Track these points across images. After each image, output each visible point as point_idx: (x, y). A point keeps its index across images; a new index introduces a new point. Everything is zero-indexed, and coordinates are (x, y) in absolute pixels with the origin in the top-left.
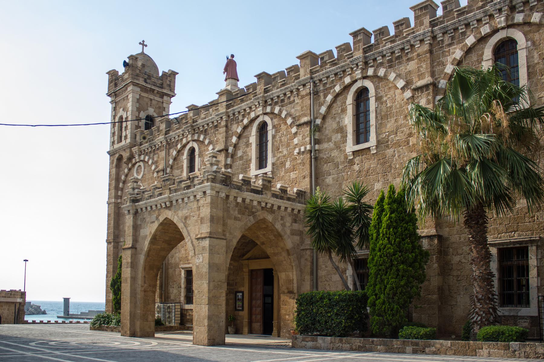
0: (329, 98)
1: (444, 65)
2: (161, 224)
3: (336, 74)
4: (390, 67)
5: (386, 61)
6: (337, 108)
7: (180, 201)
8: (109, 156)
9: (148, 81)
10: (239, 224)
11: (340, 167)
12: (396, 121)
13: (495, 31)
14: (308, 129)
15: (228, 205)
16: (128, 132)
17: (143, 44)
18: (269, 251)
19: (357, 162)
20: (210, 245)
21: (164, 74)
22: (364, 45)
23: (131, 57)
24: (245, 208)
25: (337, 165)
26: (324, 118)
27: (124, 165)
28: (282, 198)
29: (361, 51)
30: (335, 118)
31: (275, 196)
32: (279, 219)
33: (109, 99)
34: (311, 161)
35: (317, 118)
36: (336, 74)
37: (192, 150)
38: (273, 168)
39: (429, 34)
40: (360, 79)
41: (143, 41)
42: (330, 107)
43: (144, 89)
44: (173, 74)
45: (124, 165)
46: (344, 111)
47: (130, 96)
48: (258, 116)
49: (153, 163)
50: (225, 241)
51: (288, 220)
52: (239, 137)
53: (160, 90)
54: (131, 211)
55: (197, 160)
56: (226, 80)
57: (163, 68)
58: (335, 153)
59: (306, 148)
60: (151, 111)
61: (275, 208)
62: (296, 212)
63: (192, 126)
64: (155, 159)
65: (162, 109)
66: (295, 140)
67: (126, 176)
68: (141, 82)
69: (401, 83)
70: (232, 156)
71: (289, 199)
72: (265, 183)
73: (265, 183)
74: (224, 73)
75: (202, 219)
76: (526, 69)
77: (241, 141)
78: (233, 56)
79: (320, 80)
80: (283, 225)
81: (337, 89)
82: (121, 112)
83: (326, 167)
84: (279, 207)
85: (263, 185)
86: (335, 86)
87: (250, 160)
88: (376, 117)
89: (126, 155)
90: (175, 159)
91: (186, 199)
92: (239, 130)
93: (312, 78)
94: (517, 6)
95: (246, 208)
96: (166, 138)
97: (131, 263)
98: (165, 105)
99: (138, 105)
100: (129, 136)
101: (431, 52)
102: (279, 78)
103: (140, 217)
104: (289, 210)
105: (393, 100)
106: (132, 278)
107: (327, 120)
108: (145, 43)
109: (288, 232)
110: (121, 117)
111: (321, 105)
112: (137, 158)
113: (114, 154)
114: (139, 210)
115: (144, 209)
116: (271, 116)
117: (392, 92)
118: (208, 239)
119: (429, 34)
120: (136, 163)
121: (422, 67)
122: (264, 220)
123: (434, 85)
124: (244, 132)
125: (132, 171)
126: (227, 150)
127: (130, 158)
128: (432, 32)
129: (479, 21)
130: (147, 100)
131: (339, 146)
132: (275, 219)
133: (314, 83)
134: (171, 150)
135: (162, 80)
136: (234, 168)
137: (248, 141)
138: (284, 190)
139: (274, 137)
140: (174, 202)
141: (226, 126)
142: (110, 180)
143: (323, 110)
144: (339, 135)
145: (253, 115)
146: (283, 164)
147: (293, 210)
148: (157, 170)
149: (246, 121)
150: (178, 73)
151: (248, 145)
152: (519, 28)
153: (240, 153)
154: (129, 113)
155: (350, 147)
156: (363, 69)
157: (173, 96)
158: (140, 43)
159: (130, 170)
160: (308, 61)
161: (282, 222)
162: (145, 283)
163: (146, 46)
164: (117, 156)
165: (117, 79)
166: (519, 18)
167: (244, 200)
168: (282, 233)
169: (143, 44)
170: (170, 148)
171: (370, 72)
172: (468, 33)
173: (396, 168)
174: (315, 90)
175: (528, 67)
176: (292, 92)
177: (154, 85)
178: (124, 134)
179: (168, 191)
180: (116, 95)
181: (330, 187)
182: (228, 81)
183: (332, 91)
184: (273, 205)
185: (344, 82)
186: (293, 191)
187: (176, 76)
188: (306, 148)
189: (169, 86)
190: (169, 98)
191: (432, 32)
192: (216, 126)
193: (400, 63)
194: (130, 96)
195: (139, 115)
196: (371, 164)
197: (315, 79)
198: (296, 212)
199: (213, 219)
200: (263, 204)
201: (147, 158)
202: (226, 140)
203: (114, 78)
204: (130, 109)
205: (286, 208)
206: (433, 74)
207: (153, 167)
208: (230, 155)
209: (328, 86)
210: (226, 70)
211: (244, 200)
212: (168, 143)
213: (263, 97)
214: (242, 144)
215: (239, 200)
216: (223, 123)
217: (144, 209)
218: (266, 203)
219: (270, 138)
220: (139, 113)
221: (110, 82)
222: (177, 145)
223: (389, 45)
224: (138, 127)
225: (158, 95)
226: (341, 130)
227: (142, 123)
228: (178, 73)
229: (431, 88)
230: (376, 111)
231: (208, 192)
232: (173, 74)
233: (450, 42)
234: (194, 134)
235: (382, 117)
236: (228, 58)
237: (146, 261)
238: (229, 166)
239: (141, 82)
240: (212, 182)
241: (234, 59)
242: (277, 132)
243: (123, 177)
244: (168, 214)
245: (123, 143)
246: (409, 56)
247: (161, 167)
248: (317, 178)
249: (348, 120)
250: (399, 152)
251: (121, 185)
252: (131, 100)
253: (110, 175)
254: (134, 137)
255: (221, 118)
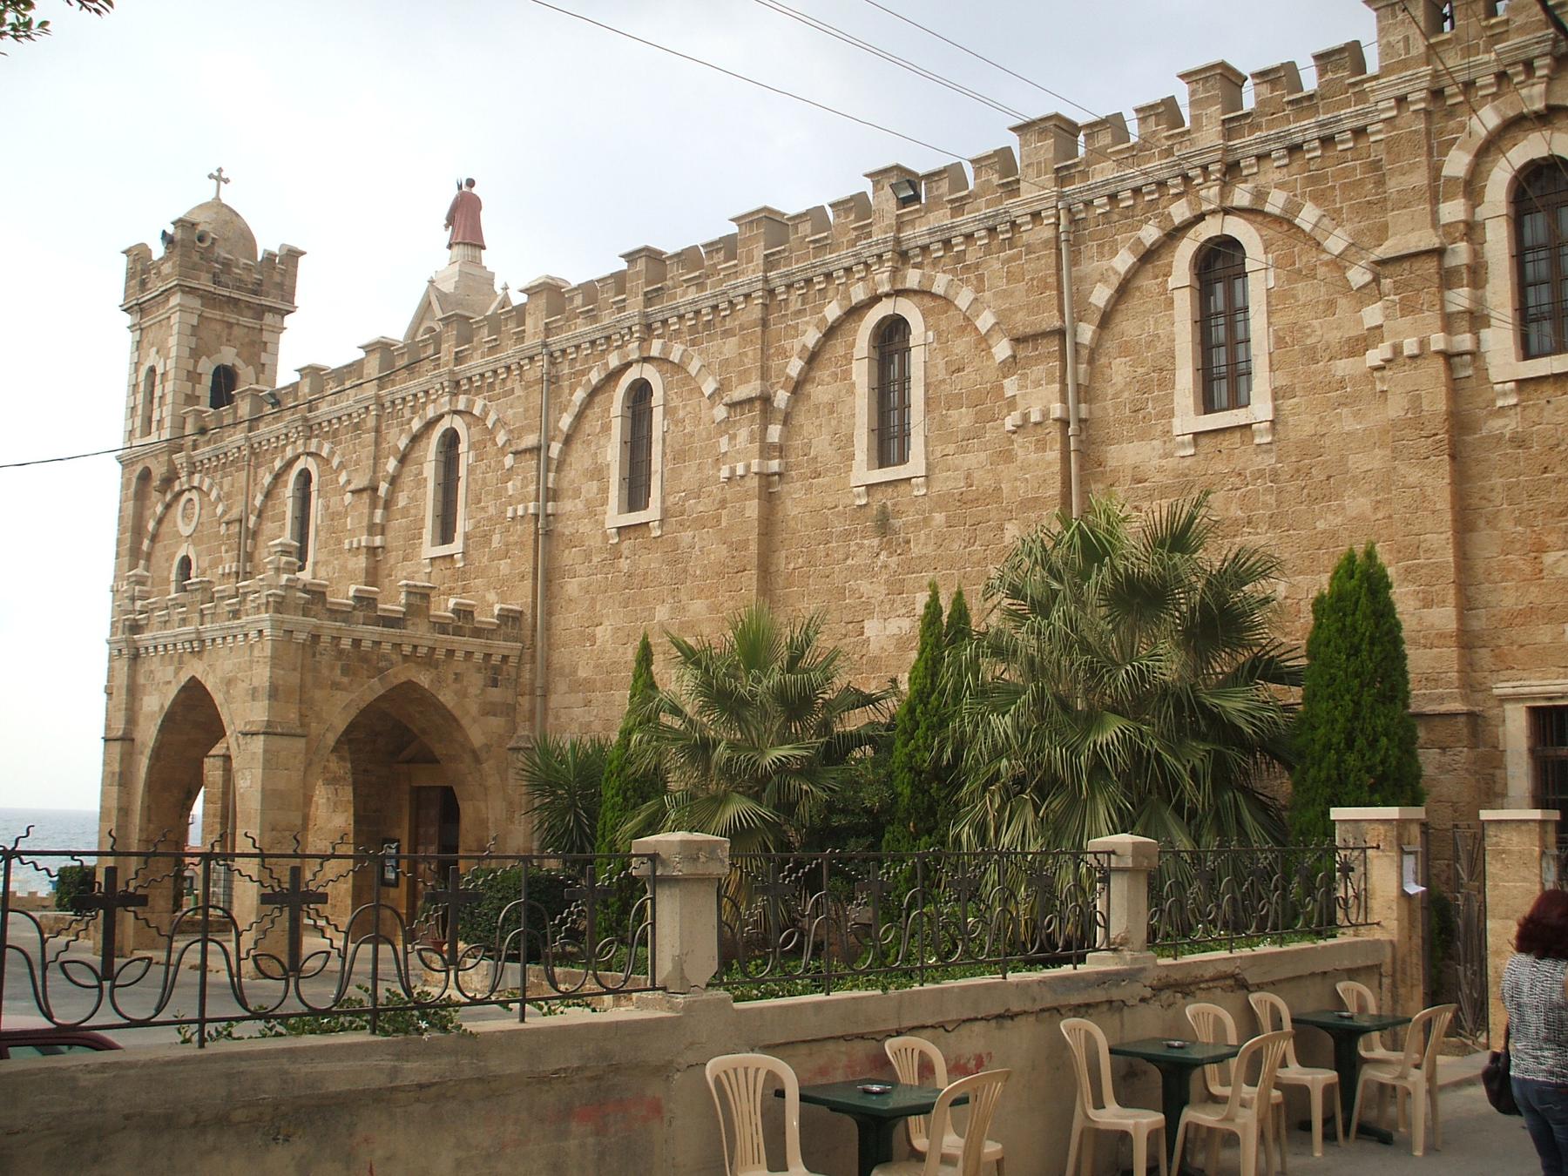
0: (579, 395)
1: (785, 354)
2: (184, 689)
3: (593, 343)
4: (693, 343)
5: (685, 329)
6: (592, 424)
7: (219, 641)
8: (119, 467)
9: (223, 278)
10: (342, 698)
11: (595, 560)
12: (700, 468)
13: (875, 299)
14: (534, 463)
15: (318, 657)
16: (167, 410)
17: (219, 178)
18: (439, 750)
19: (626, 553)
20: (265, 751)
21: (270, 257)
22: (648, 283)
23: (179, 223)
24: (359, 660)
25: (588, 557)
26: (568, 441)
27: (155, 495)
28: (458, 631)
29: (641, 298)
30: (589, 445)
31: (441, 627)
32: (450, 681)
33: (127, 319)
34: (536, 541)
35: (553, 439)
36: (593, 343)
37: (305, 476)
38: (466, 545)
39: (760, 285)
40: (637, 361)
41: (220, 170)
42: (579, 417)
43: (209, 299)
44: (293, 255)
45: (155, 495)
46: (606, 428)
47: (175, 319)
48: (442, 416)
49: (219, 498)
50: (303, 740)
51: (474, 682)
52: (403, 460)
53: (255, 300)
54: (125, 651)
55: (316, 504)
56: (450, 246)
57: (267, 241)
58: (585, 527)
59: (526, 509)
60: (228, 356)
61: (440, 654)
62: (496, 659)
63: (306, 420)
64: (226, 488)
65: (260, 349)
66: (510, 484)
67: (160, 521)
68: (204, 282)
69: (709, 386)
70: (387, 505)
71: (478, 632)
72: (413, 599)
73: (413, 599)
74: (447, 227)
75: (255, 690)
76: (922, 389)
77: (406, 469)
78: (471, 183)
79: (564, 351)
80: (463, 694)
81: (595, 377)
82: (152, 359)
83: (569, 557)
84: (450, 653)
85: (408, 605)
86: (591, 368)
87: (423, 519)
88: (664, 454)
89: (159, 470)
90: (268, 495)
91: (230, 639)
92: (403, 443)
93: (545, 345)
94: (911, 253)
95: (364, 659)
96: (248, 439)
97: (121, 774)
98: (266, 336)
99: (193, 342)
100: (167, 423)
101: (764, 323)
102: (486, 331)
103: (143, 669)
104: (478, 656)
105: (698, 420)
106: (120, 809)
107: (574, 447)
108: (224, 175)
109: (474, 709)
110: (152, 370)
111: (563, 409)
112: (184, 479)
113: (132, 464)
114: (142, 651)
115: (151, 649)
116: (468, 418)
117: (694, 402)
118: (262, 737)
119: (760, 285)
120: (182, 492)
121: (745, 354)
122: (411, 685)
123: (766, 400)
124: (412, 449)
125: (173, 510)
126: (375, 489)
127: (168, 481)
128: (766, 280)
129: (848, 270)
130: (218, 327)
131: (593, 510)
132: (439, 680)
133: (551, 355)
134: (261, 471)
135: (260, 273)
136: (390, 534)
137: (421, 473)
138: (464, 613)
139: (471, 470)
140: (208, 643)
141: (377, 430)
142: (122, 531)
143: (565, 422)
144: (595, 485)
145: (431, 412)
146: (486, 538)
147: (488, 656)
148: (226, 519)
149: (416, 425)
150: (303, 253)
151: (420, 482)
152: (916, 299)
153: (402, 500)
154: (171, 364)
155: (615, 516)
156: (642, 340)
157: (289, 312)
158: (211, 176)
159: (168, 507)
160: (542, 301)
161: (458, 686)
162: (149, 821)
163: (226, 181)
164: (139, 468)
165: (145, 271)
166: (913, 278)
167: (357, 643)
168: (457, 713)
169: (219, 178)
170: (258, 466)
171: (656, 348)
172: (830, 293)
173: (695, 576)
174: (553, 372)
175: (927, 386)
176: (508, 368)
177: (239, 288)
178: (156, 416)
179: (196, 616)
180: (141, 310)
181: (573, 605)
182: (456, 249)
183: (584, 379)
184: (432, 650)
185: (607, 364)
186: (487, 616)
187: (301, 259)
188: (526, 509)
189: (281, 285)
190: (278, 317)
191: (766, 280)
192: (357, 427)
193: (711, 338)
194: (175, 319)
195: (195, 366)
196: (652, 561)
197: (554, 348)
198: (496, 659)
199: (274, 693)
200: (407, 649)
201: (207, 481)
202: (375, 464)
203: (139, 263)
204: (173, 353)
205: (469, 654)
206: (765, 374)
207: (219, 510)
208: (381, 503)
209: (578, 367)
210: (451, 220)
211: (357, 643)
212: (253, 452)
213: (451, 372)
214: (407, 479)
215: (346, 644)
216: (371, 422)
217: (151, 649)
218: (415, 647)
219: (462, 471)
220: (196, 362)
221: (131, 275)
222: (273, 461)
223: (692, 294)
224: (191, 399)
225: (250, 313)
226: (598, 473)
227: (204, 389)
228: (303, 253)
229: (758, 404)
230: (664, 440)
231: (267, 632)
232: (293, 255)
233: (799, 306)
234: (309, 438)
235: (679, 456)
236: (460, 187)
237: (150, 769)
238: (379, 530)
239: (204, 282)
240: (277, 611)
241: (475, 190)
242: (479, 458)
243: (151, 525)
244: (196, 668)
245: (154, 438)
246: (728, 324)
247: (235, 513)
248: (548, 581)
249: (612, 452)
250: (702, 539)
251: (146, 544)
252: (175, 329)
253: (121, 518)
254: (179, 423)
255: (367, 408)
